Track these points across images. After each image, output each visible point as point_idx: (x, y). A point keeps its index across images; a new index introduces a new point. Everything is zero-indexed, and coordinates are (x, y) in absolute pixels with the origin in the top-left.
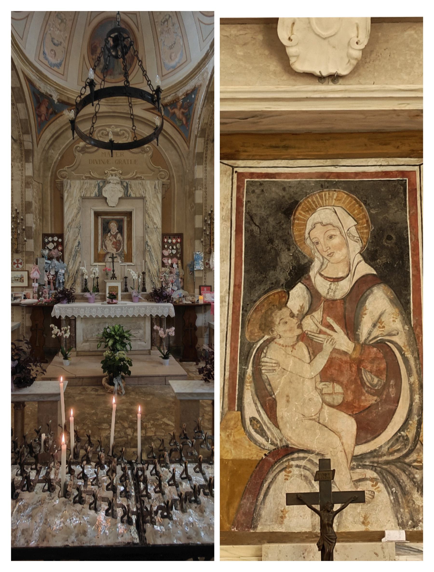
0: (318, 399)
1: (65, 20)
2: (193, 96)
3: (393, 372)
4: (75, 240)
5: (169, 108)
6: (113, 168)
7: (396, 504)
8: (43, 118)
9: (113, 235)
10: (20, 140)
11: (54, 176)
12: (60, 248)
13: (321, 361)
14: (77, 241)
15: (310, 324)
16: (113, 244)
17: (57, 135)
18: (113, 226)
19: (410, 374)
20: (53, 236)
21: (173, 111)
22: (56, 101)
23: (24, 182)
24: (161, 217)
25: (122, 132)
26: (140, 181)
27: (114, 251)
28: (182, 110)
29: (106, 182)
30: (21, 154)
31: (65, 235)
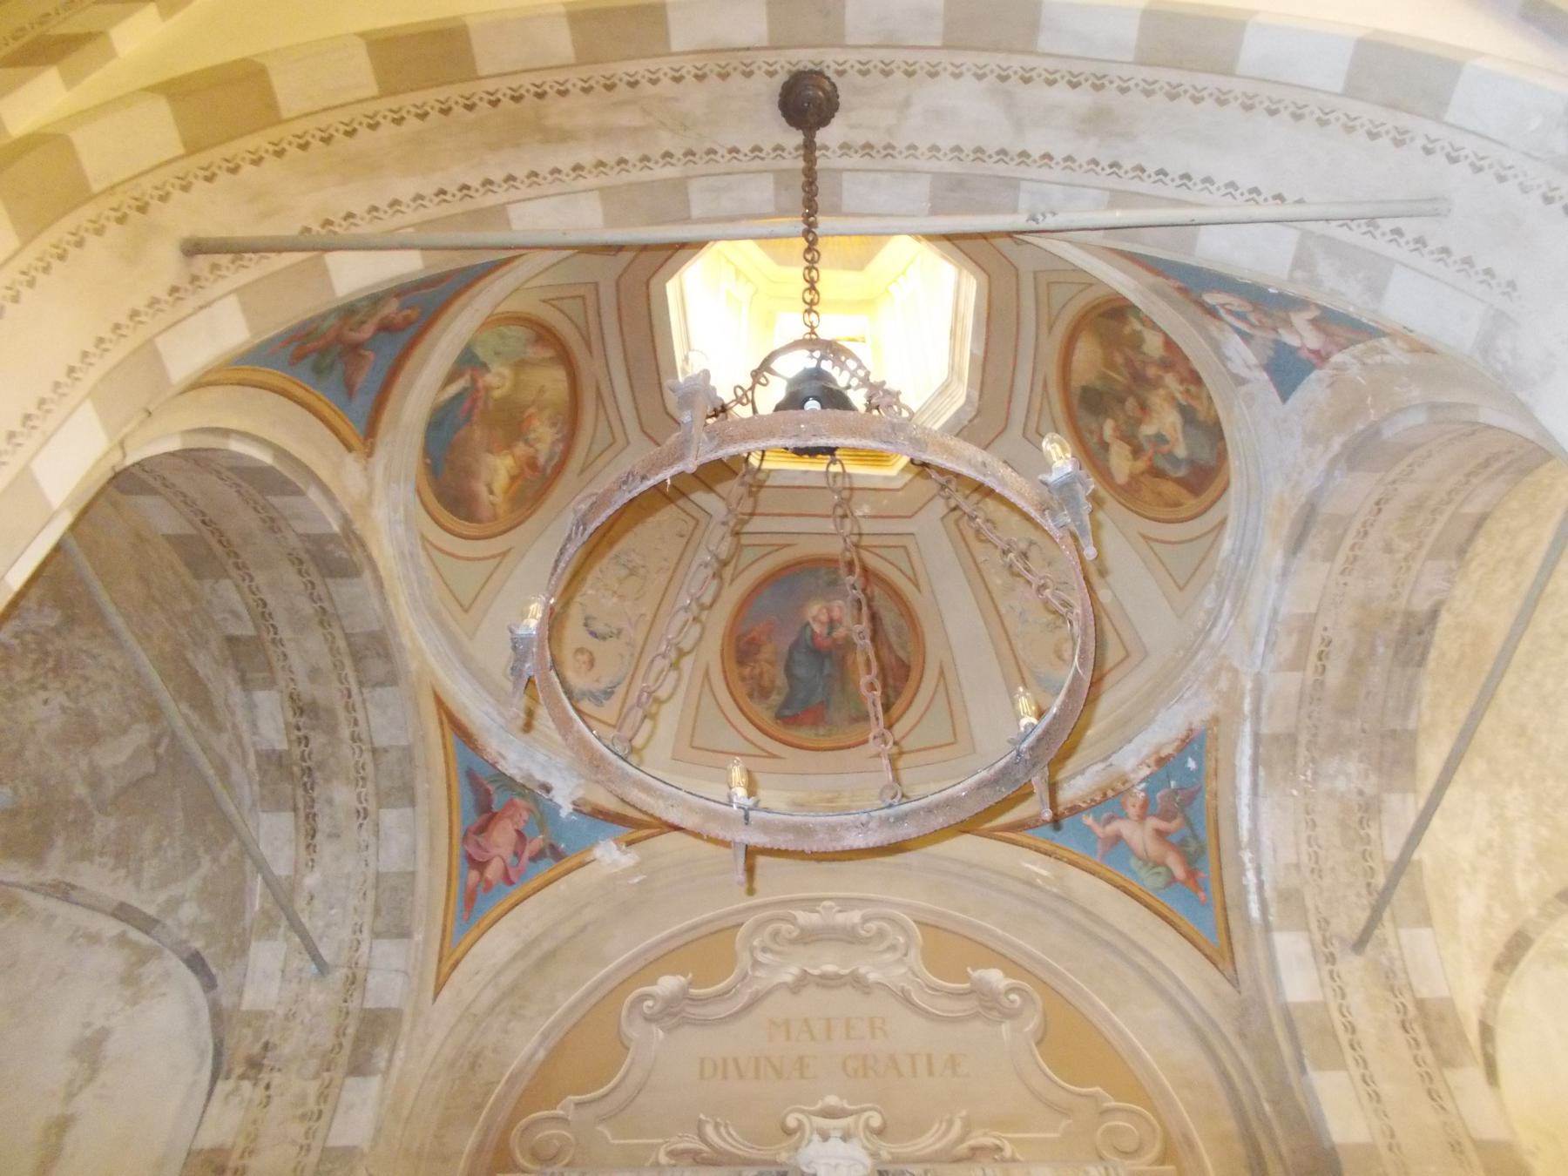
1: (642, 571)
2: (1191, 764)
6: (832, 1100)
10: (353, 965)
21: (1110, 829)
22: (566, 810)
25: (873, 926)
28: (1153, 823)
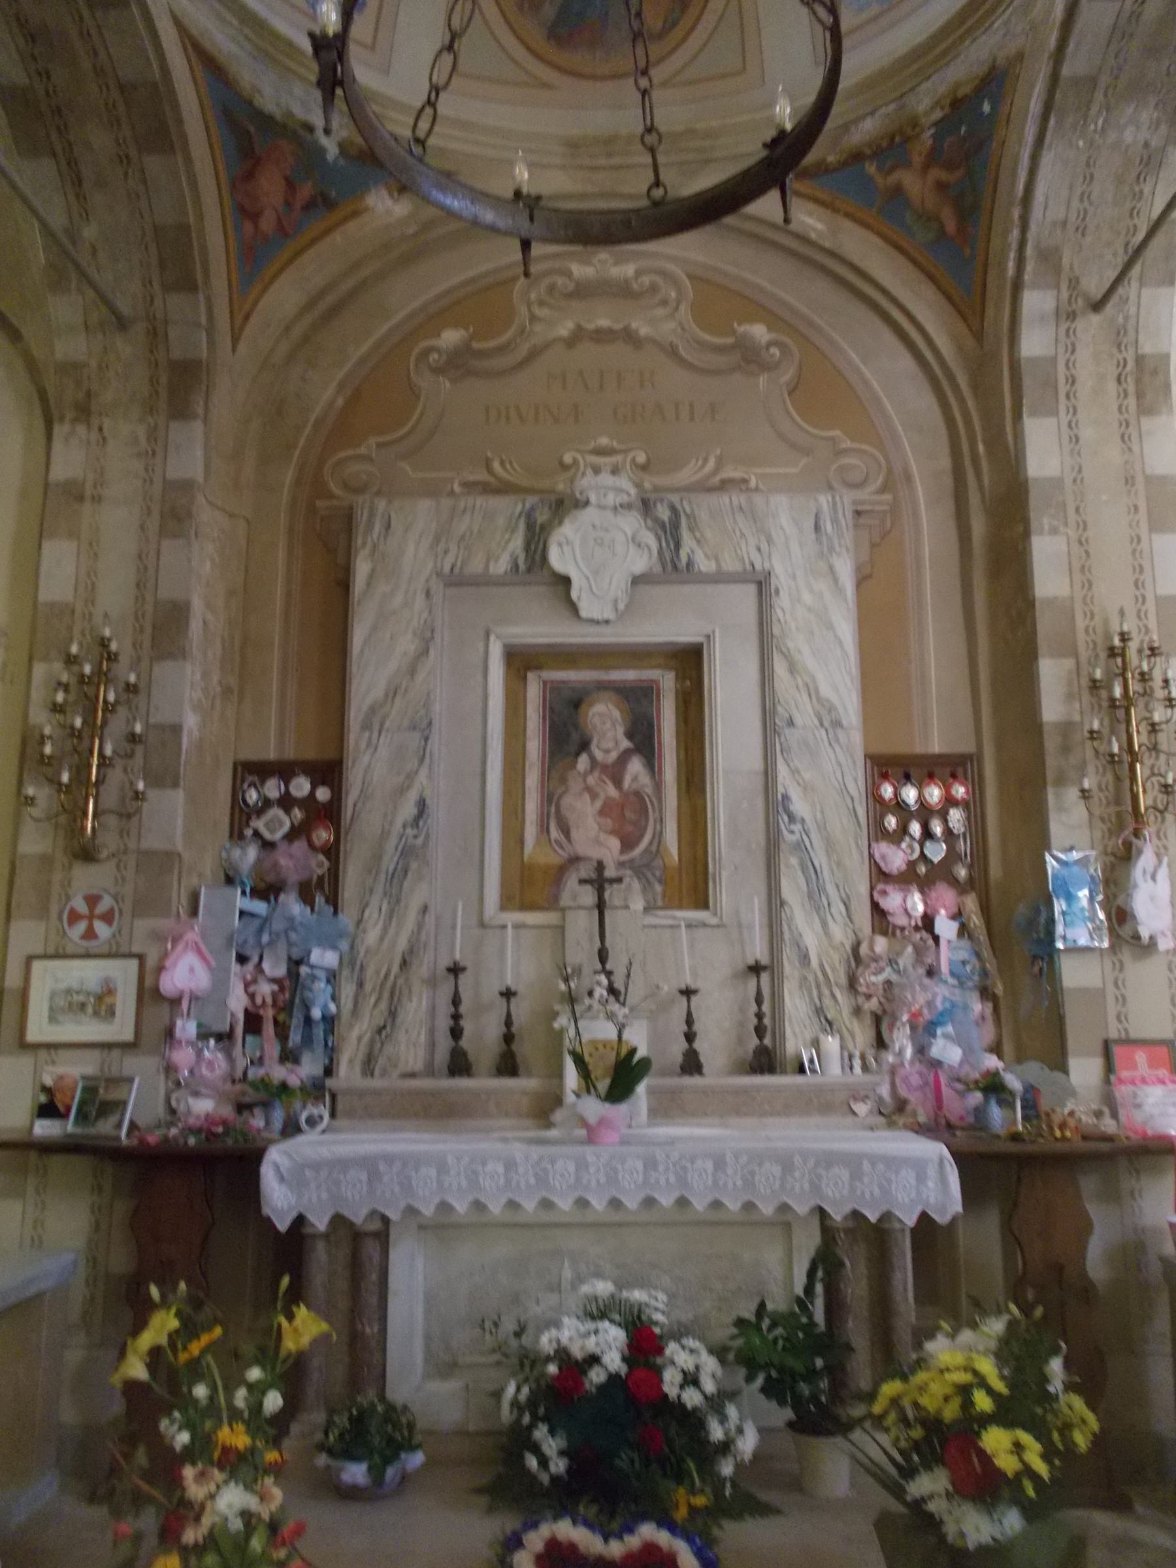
0: (596, 827)
2: (986, 108)
3: (644, 811)
4: (402, 790)
5: (871, 168)
6: (604, 441)
7: (644, 890)
8: (267, 223)
9: (604, 768)
11: (313, 485)
12: (323, 835)
13: (598, 804)
14: (412, 796)
15: (591, 780)
16: (602, 813)
17: (330, 299)
18: (606, 723)
19: (654, 812)
20: (285, 770)
23: (156, 509)
24: (855, 671)
26: (738, 499)
27: (609, 850)
28: (936, 173)
29: (564, 505)
30: (153, 381)
31: (348, 762)
